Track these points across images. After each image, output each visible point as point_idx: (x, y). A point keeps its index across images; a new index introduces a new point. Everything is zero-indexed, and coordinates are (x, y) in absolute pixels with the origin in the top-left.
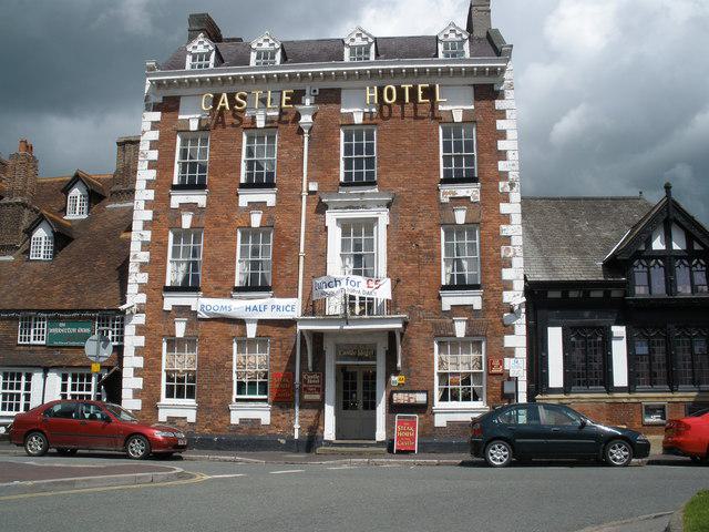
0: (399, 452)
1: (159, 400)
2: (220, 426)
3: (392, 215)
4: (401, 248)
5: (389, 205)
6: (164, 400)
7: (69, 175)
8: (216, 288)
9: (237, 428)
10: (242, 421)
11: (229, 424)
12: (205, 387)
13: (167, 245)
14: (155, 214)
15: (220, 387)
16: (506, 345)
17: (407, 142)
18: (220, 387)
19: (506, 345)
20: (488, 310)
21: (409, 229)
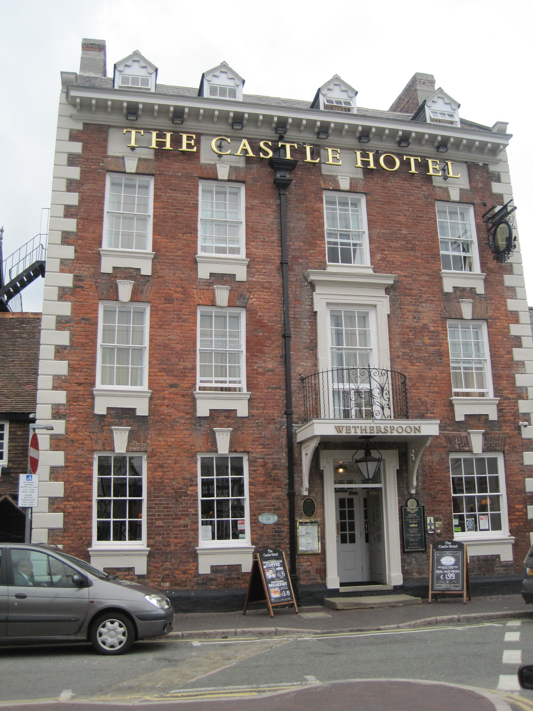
0: (435, 596)
1: (90, 544)
2: (184, 577)
3: (392, 302)
4: (404, 344)
5: (388, 289)
6: (97, 545)
7: (138, 119)
8: (172, 386)
9: (206, 580)
10: (215, 569)
11: (197, 575)
12: (160, 523)
13: (96, 324)
14: (77, 278)
15: (182, 522)
16: (526, 463)
17: (402, 219)
18: (182, 522)
19: (526, 463)
20: (505, 421)
21: (410, 322)
